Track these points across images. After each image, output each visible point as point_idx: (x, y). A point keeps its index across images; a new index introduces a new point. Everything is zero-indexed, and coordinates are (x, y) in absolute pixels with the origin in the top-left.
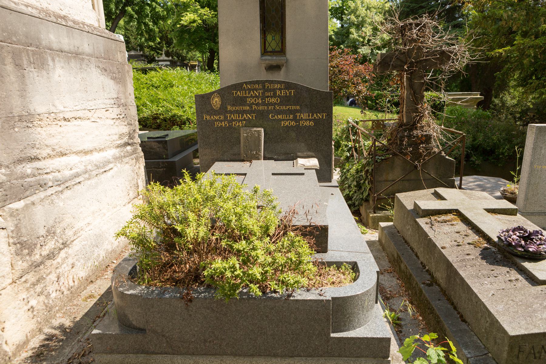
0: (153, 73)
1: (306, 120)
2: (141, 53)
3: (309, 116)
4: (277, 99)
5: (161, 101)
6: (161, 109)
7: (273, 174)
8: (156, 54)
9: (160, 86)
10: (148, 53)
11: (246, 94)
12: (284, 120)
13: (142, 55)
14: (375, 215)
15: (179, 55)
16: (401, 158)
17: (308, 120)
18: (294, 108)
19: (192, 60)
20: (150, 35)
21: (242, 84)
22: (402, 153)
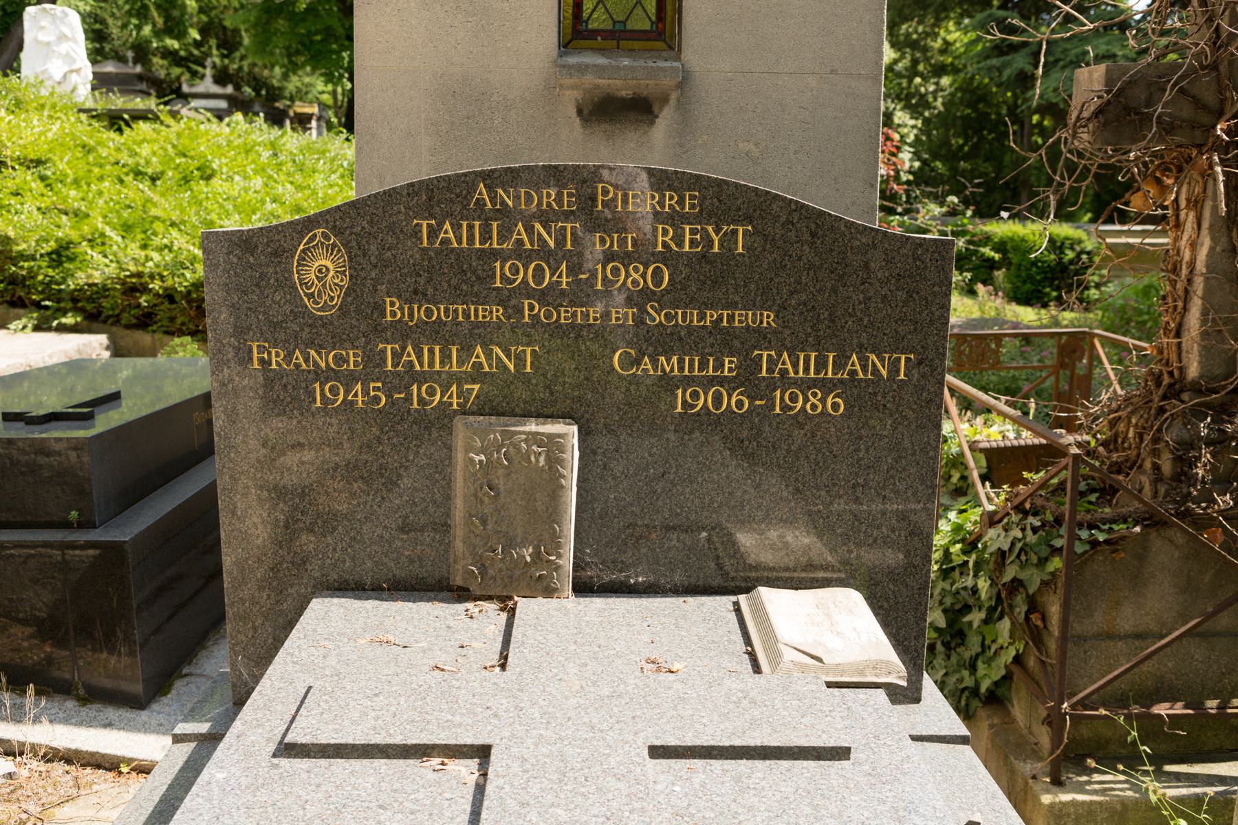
0: (143, 127)
1: (806, 385)
2: (139, 69)
3: (821, 365)
4: (657, 273)
5: (158, 226)
6: (156, 256)
7: (657, 752)
8: (187, 76)
9: (162, 173)
10: (162, 74)
11: (486, 237)
12: (688, 381)
13: (140, 78)
14: (1066, 797)
15: (258, 84)
16: (1180, 539)
17: (814, 383)
18: (743, 318)
19: (301, 99)
20: (168, 18)
21: (466, 182)
22: (1185, 515)
